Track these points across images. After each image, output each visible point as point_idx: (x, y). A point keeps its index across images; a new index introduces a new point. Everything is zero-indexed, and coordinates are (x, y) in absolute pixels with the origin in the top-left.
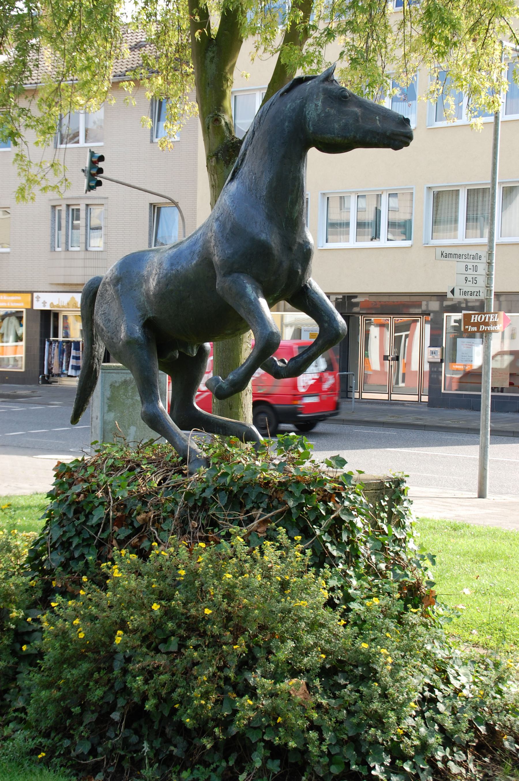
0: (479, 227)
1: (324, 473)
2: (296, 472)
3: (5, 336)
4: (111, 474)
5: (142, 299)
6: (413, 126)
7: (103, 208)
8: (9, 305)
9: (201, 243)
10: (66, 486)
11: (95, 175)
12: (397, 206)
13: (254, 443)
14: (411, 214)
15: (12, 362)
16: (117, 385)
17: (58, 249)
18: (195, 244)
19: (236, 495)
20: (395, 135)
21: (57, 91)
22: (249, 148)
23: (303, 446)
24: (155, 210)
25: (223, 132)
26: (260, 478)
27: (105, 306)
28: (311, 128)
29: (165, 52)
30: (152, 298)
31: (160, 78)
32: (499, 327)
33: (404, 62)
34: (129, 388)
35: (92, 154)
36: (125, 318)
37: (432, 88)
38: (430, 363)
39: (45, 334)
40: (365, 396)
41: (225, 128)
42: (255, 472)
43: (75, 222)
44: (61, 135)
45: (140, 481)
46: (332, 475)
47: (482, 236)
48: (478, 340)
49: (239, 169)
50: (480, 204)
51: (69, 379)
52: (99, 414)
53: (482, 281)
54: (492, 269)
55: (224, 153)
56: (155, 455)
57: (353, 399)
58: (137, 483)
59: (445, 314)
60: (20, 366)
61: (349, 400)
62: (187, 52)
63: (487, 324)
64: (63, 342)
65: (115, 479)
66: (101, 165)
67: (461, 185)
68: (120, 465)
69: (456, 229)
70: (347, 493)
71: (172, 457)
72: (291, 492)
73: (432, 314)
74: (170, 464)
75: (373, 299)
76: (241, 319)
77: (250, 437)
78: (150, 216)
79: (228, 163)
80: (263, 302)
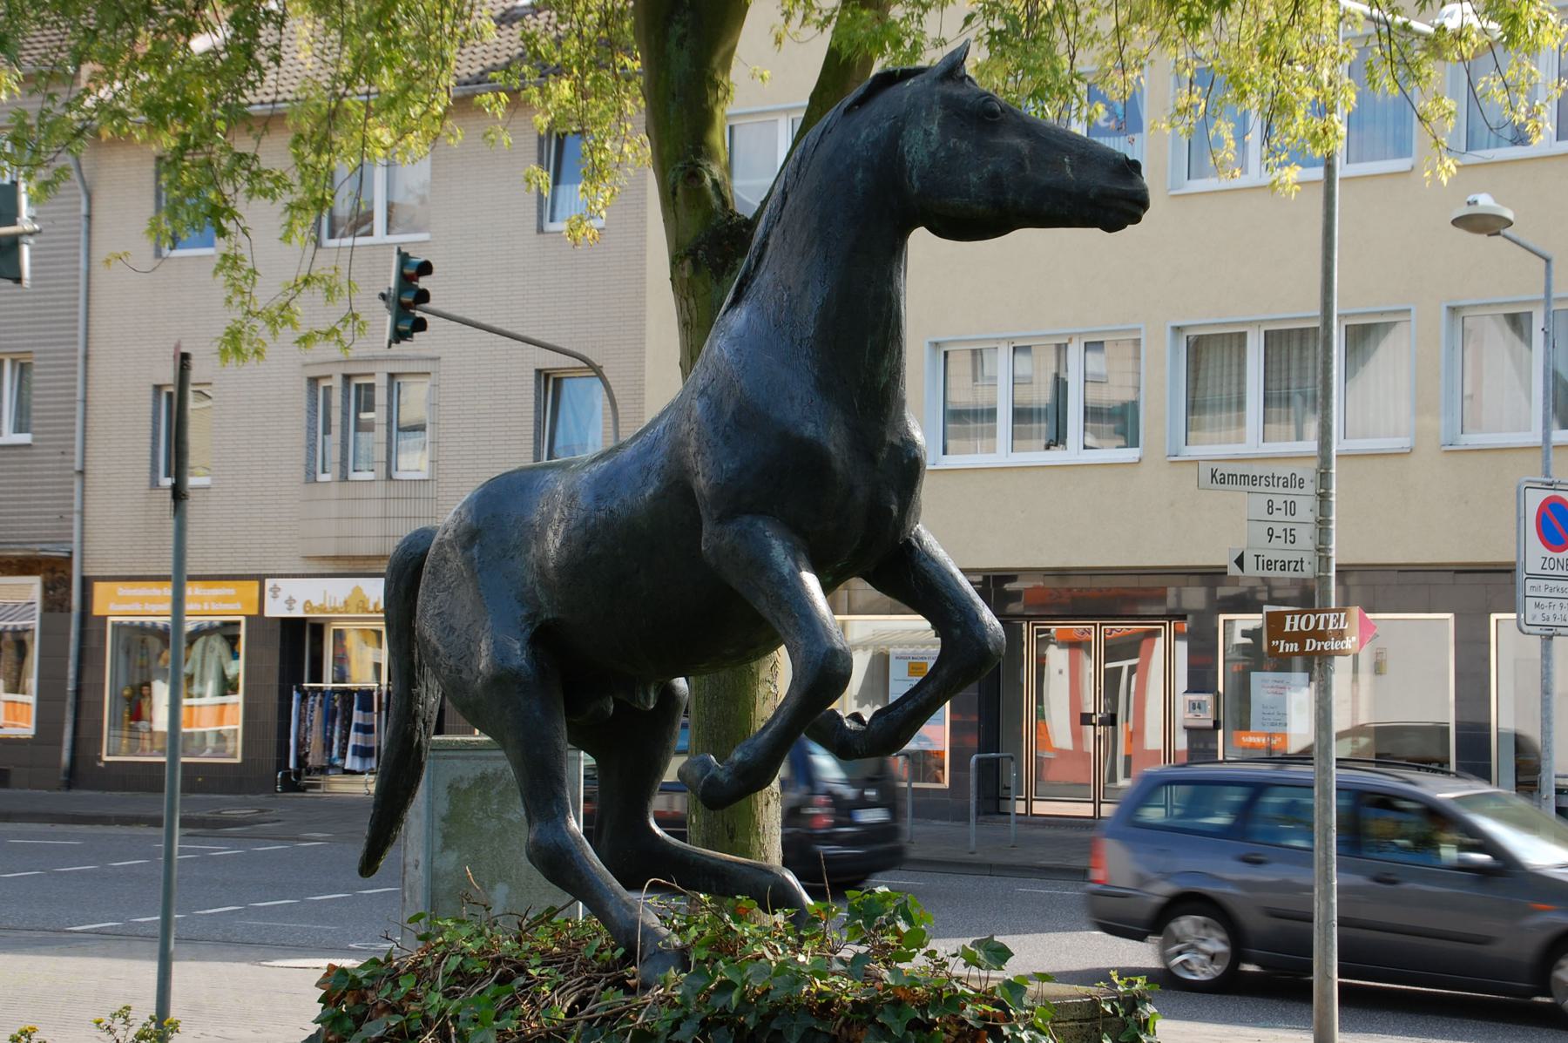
0: (1292, 417)
1: (958, 979)
2: (892, 977)
3: (196, 680)
4: (456, 992)
5: (529, 578)
6: (1148, 177)
7: (427, 381)
8: (206, 607)
9: (664, 446)
10: (349, 1024)
11: (409, 304)
12: (1104, 371)
13: (791, 912)
14: (1138, 389)
15: (211, 742)
16: (465, 786)
17: (322, 477)
18: (651, 449)
19: (752, 1034)
20: (1104, 195)
21: (333, 117)
22: (775, 230)
23: (908, 919)
24: (549, 384)
25: (708, 202)
26: (809, 992)
27: (442, 596)
28: (917, 185)
29: (575, 26)
30: (552, 575)
31: (566, 83)
32: (1350, 643)
33: (1115, 44)
34: (493, 792)
35: (404, 258)
36: (489, 624)
37: (1183, 102)
38: (1191, 730)
39: (290, 675)
40: (1040, 808)
41: (711, 193)
42: (797, 979)
43: (363, 416)
44: (332, 219)
45: (525, 1006)
46: (977, 987)
47: (1300, 437)
48: (1299, 677)
49: (753, 279)
50: (1294, 364)
51: (348, 778)
52: (421, 857)
53: (1306, 538)
54: (1330, 508)
55: (712, 249)
56: (560, 944)
57: (1013, 817)
58: (517, 1012)
59: (1222, 617)
60: (230, 751)
61: (1003, 818)
62: (627, 25)
63: (1321, 636)
64: (334, 691)
65: (467, 1003)
66: (423, 283)
67: (1250, 323)
68: (478, 970)
69: (1241, 422)
70: (1014, 1028)
71: (601, 949)
72: (882, 1025)
73: (1190, 617)
74: (597, 965)
75: (1053, 583)
76: (758, 621)
77: (781, 898)
78: (537, 398)
79: (721, 269)
80: (811, 581)
